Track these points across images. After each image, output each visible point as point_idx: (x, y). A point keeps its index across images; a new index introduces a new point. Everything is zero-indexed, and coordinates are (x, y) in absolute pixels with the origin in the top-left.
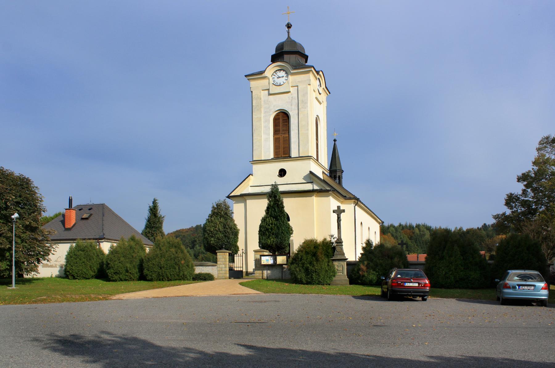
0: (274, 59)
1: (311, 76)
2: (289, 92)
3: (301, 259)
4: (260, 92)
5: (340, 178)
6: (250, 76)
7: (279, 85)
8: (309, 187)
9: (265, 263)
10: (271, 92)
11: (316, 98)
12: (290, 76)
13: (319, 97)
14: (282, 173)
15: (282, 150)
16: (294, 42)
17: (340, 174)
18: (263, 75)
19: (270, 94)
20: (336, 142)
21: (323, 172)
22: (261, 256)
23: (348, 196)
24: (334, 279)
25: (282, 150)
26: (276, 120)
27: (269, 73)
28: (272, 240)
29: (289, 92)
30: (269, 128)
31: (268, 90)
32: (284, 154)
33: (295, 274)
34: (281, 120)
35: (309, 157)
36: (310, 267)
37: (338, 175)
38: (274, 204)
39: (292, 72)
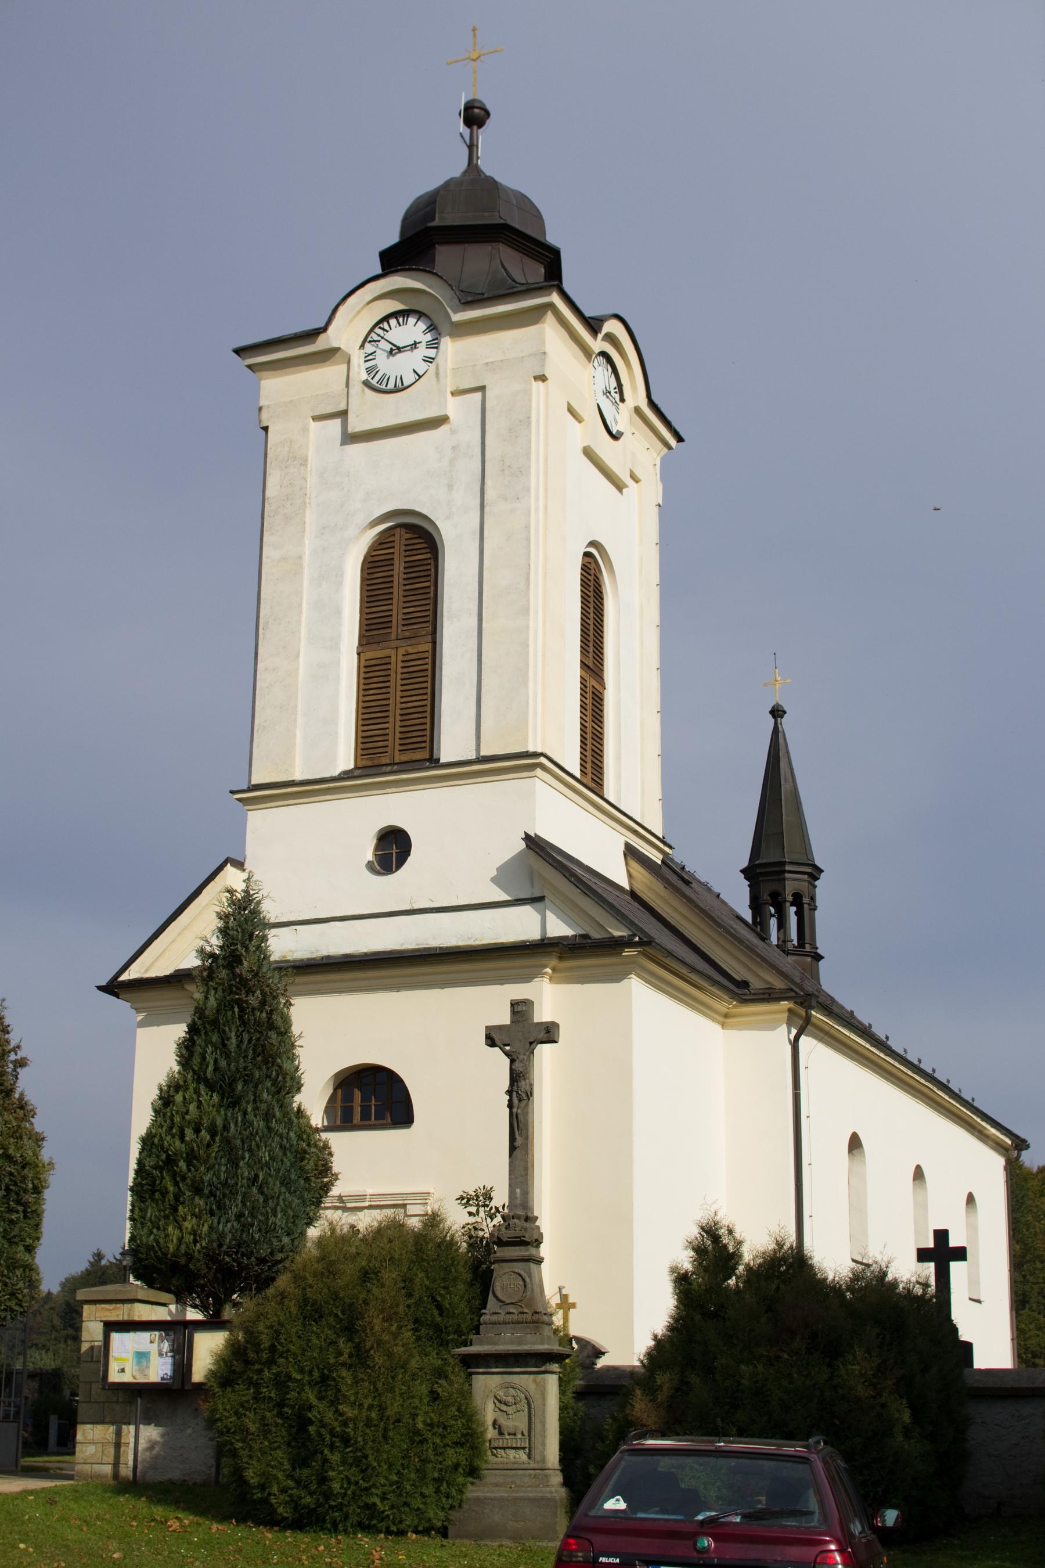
0: (392, 261)
1: (552, 338)
2: (440, 421)
3: (273, 1349)
4: (305, 430)
5: (805, 905)
6: (265, 352)
7: (396, 390)
8: (522, 925)
9: (127, 1378)
10: (356, 425)
11: (588, 453)
12: (446, 342)
13: (605, 447)
14: (393, 848)
15: (398, 731)
16: (492, 186)
17: (804, 887)
18: (322, 343)
19: (350, 438)
20: (785, 722)
21: (630, 852)
22: (111, 1327)
23: (756, 984)
24: (472, 1492)
25: (398, 731)
26: (375, 569)
27: (347, 331)
28: (187, 1231)
29: (440, 421)
30: (338, 612)
31: (343, 414)
32: (405, 747)
33: (234, 1454)
34: (399, 568)
35: (525, 762)
36: (321, 1411)
37: (790, 888)
38: (224, 1006)
39: (456, 317)
